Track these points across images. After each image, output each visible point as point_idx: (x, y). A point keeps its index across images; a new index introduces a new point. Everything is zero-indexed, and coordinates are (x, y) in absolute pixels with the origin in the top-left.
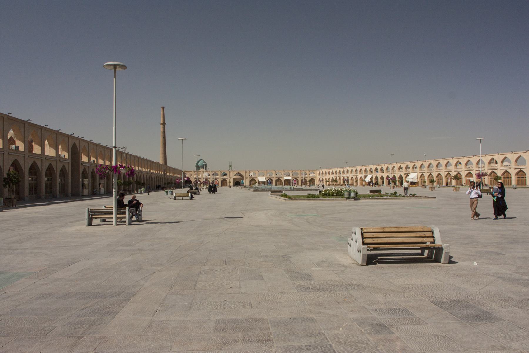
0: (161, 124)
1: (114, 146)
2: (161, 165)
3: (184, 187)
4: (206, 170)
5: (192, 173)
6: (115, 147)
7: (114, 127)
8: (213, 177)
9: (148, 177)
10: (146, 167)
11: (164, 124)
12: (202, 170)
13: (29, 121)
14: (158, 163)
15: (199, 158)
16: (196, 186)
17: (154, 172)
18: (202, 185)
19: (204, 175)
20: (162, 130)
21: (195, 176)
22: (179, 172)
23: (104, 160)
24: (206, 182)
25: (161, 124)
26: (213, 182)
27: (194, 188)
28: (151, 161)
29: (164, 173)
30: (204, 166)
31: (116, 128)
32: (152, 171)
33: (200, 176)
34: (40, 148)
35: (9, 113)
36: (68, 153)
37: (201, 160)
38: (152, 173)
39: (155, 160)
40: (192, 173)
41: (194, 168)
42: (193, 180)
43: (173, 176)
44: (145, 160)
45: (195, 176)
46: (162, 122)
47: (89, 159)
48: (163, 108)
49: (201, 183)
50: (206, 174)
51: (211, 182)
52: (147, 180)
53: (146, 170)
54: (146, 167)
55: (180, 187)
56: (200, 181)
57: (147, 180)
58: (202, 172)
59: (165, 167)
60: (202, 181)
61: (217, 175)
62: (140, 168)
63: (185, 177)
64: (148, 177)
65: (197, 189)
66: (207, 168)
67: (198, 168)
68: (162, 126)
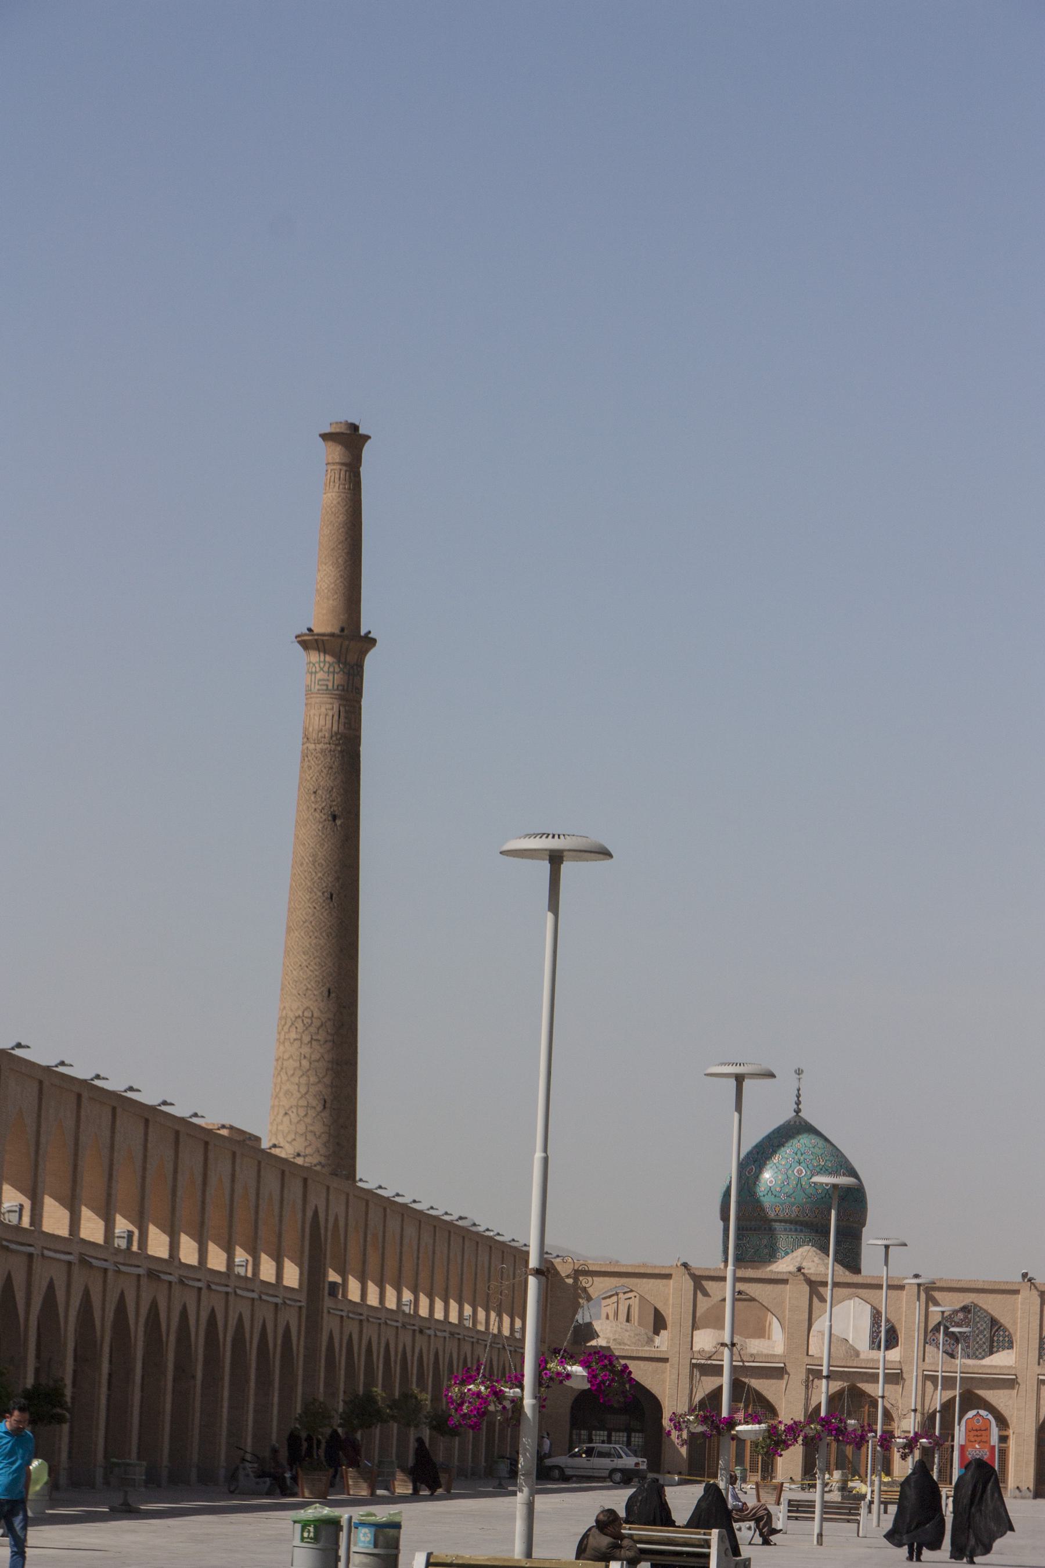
0: (310, 642)
1: (880, 1394)
2: (285, 1168)
3: (549, 1476)
4: (849, 1257)
5: (672, 1298)
6: (883, 1397)
7: (539, 1155)
8: (937, 1360)
9: (429, 1361)
10: (91, 1179)
11: (345, 648)
12: (800, 1258)
13: (97, 1083)
14: (243, 1144)
15: (768, 1111)
16: (699, 1466)
17: (188, 1252)
18: (789, 1462)
19: (820, 1332)
20: (321, 716)
21: (705, 1340)
22: (478, 1260)
23: (415, 1293)
24: (842, 1429)
25: (310, 642)
26: (936, 1429)
27: (683, 1499)
28: (150, 1116)
29: (313, 1276)
30: (838, 1217)
31: (546, 1160)
32: (158, 1245)
33: (774, 1344)
34: (165, 1239)
35: (165, 1103)
36: (300, 1265)
37: (796, 1128)
38: (155, 1271)
39: (213, 1109)
40: (672, 1298)
41: (707, 1244)
42: (673, 1394)
43: (422, 1328)
44: (84, 1094)
45: (705, 1340)
46: (319, 615)
47: (174, 1246)
48: (350, 441)
49: (776, 1442)
50: (849, 1320)
51: (908, 1425)
52: (86, 1355)
53: (92, 1229)
54: (91, 1179)
55: (493, 1474)
56: (762, 1408)
57: (86, 1355)
58: (796, 1294)
59: (319, 1195)
60: (790, 1404)
61: (996, 1336)
62: (241, 1256)
63: (566, 1336)
64: (429, 1361)
65: (715, 1512)
66: (871, 1241)
67: (754, 1232)
68: (308, 675)
